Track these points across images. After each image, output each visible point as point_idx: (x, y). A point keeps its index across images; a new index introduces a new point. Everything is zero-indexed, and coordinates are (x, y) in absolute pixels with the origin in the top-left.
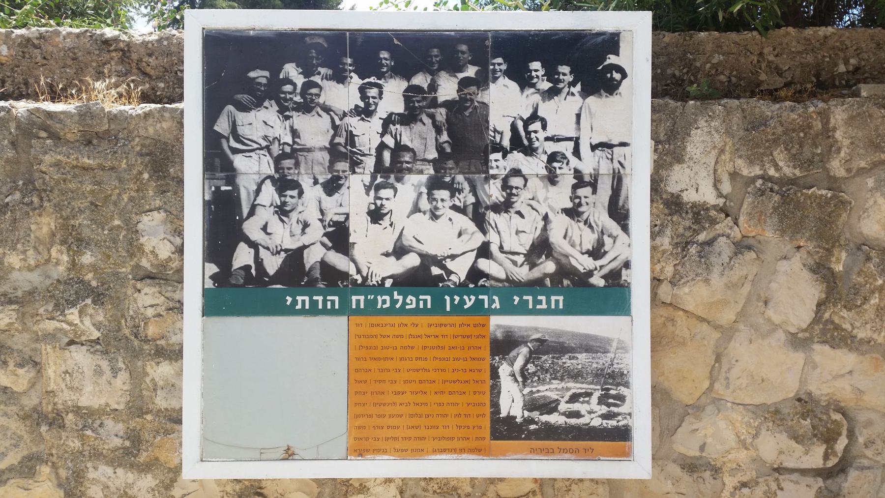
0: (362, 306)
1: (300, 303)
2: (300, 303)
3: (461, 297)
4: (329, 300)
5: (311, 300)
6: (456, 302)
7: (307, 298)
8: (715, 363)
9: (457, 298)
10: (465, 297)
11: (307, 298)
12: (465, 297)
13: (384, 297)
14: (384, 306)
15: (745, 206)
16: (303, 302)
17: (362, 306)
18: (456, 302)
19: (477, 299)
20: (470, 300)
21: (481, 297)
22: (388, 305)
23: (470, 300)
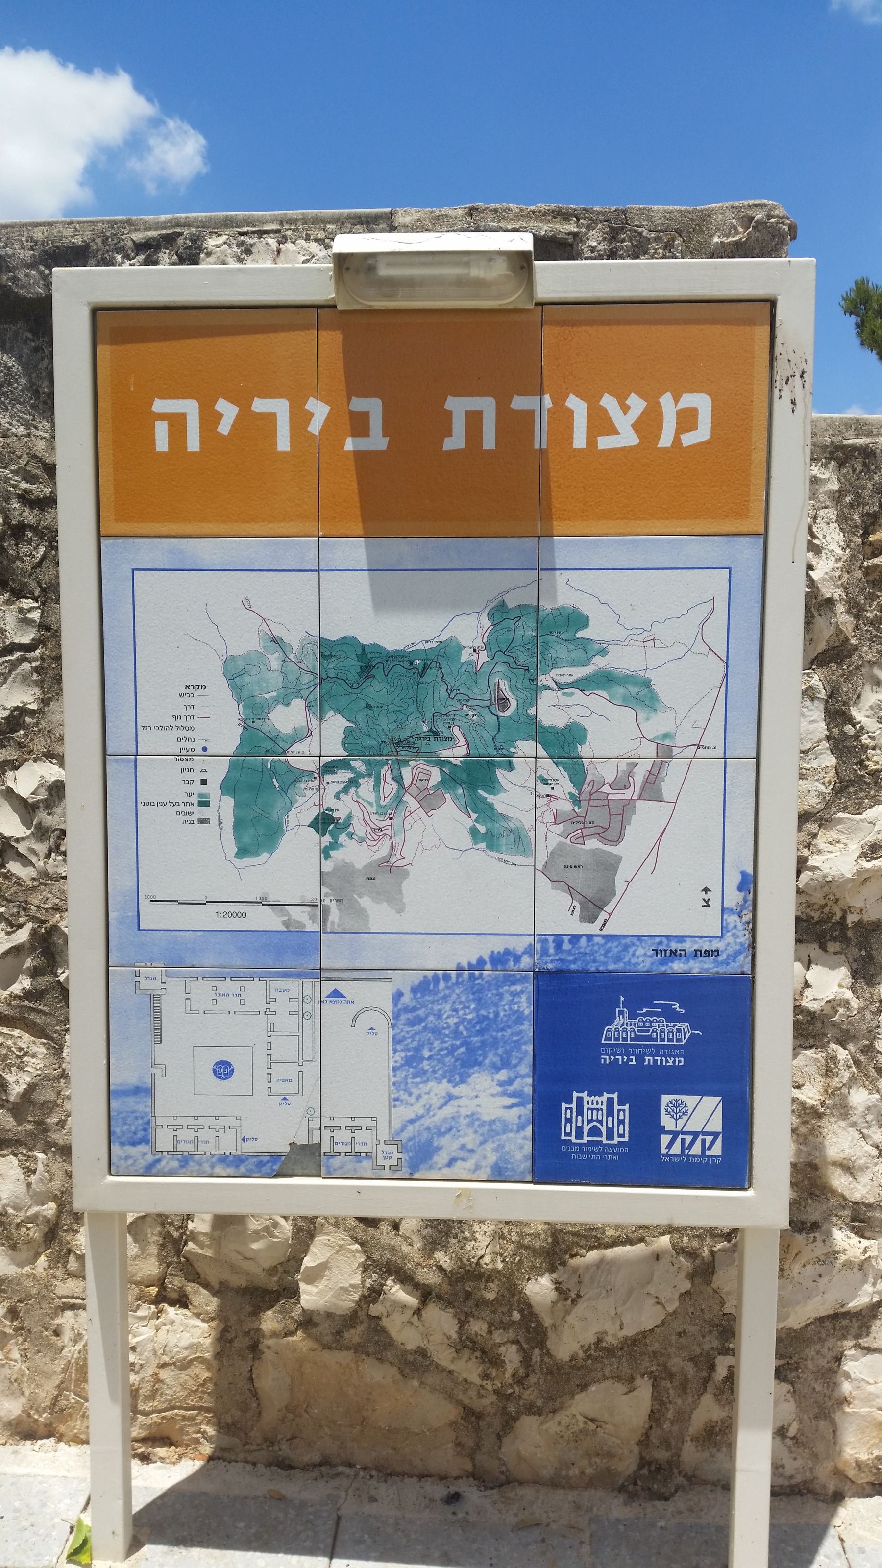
0: (489, 441)
1: (459, 425)
2: (459, 425)
3: (243, 401)
4: (162, 417)
5: (503, 412)
6: (224, 428)
7: (487, 406)
8: (300, 776)
9: (228, 411)
10: (609, 402)
11: (487, 406)
12: (609, 402)
13: (688, 400)
14: (689, 439)
15: (32, 1006)
16: (474, 419)
17: (489, 441)
18: (224, 428)
19: (245, 416)
20: (625, 409)
21: (260, 405)
22: (702, 433)
23: (625, 409)
